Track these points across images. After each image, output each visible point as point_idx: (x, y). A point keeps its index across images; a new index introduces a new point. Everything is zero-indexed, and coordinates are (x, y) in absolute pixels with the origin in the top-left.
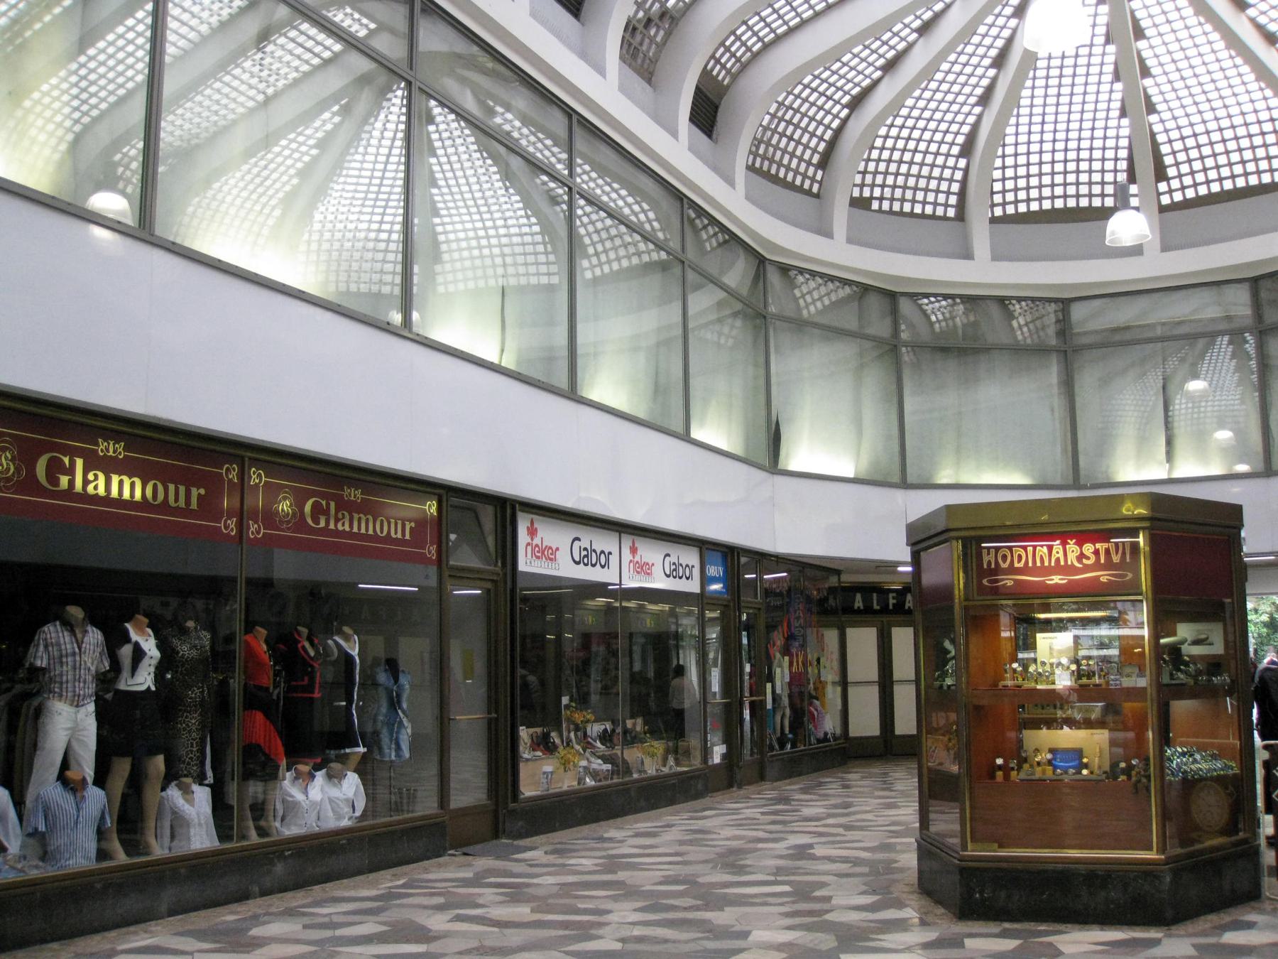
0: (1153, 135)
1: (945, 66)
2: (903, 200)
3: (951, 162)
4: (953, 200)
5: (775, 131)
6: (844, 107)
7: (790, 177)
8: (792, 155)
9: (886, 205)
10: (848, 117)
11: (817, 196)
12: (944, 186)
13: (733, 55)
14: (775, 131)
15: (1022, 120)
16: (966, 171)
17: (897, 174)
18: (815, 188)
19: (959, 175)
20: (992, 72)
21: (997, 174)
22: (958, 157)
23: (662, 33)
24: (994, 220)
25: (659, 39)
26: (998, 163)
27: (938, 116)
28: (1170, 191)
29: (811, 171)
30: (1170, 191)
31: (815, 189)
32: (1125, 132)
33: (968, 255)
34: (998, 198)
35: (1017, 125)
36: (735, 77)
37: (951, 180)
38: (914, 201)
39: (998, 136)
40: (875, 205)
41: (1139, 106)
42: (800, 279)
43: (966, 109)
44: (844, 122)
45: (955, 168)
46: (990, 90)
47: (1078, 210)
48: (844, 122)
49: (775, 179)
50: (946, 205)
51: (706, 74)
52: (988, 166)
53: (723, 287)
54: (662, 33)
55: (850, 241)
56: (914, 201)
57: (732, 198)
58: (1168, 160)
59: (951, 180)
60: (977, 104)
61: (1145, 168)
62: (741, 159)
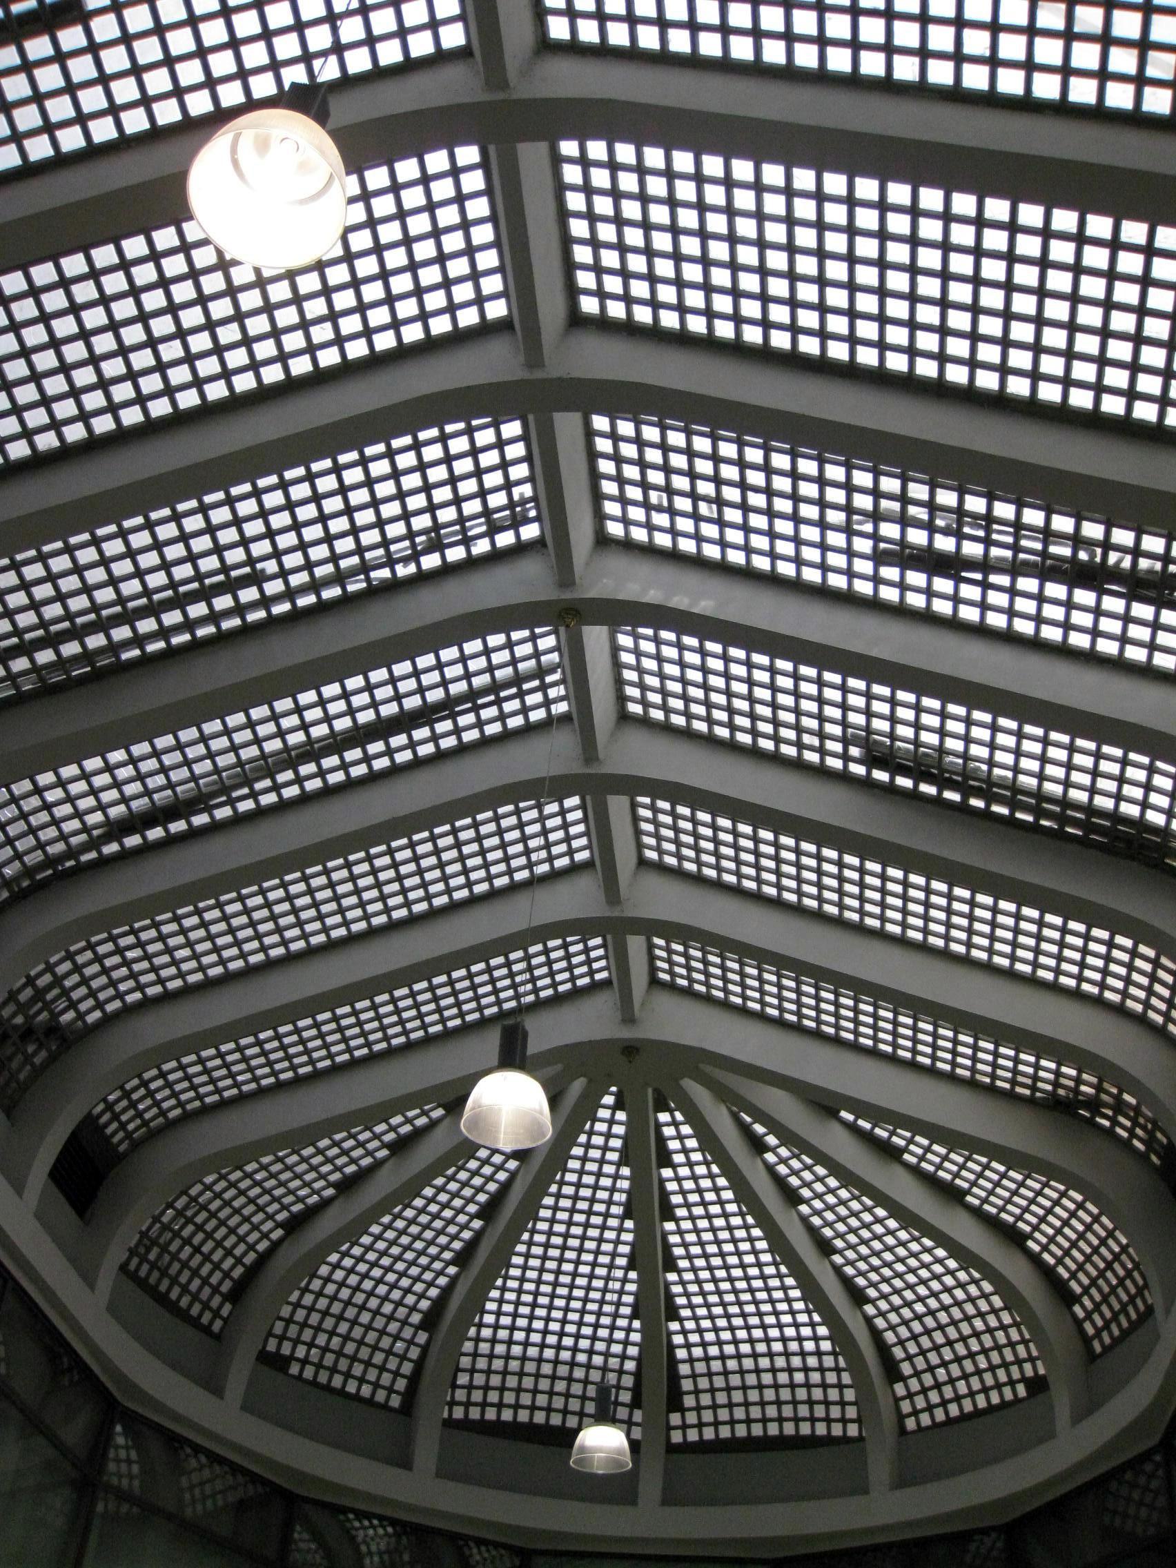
2: (333, 1370)
3: (407, 1333)
4: (401, 1384)
5: (177, 1234)
6: (278, 1225)
7: (184, 1302)
8: (195, 1273)
9: (309, 1373)
10: (281, 1241)
13: (139, 1115)
14: (177, 1234)
16: (425, 1349)
17: (332, 1333)
18: (217, 1326)
19: (414, 1353)
22: (418, 1328)
23: (43, 1054)
24: (449, 1423)
25: (37, 1060)
28: (684, 1427)
29: (217, 1300)
33: (405, 1463)
36: (136, 1145)
37: (403, 1358)
38: (348, 1375)
40: (294, 1369)
41: (655, 1308)
42: (193, 1463)
45: (411, 1342)
49: (162, 1299)
50: (390, 1390)
51: (89, 1124)
53: (56, 1443)
54: (43, 1054)
56: (348, 1375)
57: (87, 1308)
58: (687, 1385)
59: (403, 1358)
61: (657, 1392)
62: (116, 1254)
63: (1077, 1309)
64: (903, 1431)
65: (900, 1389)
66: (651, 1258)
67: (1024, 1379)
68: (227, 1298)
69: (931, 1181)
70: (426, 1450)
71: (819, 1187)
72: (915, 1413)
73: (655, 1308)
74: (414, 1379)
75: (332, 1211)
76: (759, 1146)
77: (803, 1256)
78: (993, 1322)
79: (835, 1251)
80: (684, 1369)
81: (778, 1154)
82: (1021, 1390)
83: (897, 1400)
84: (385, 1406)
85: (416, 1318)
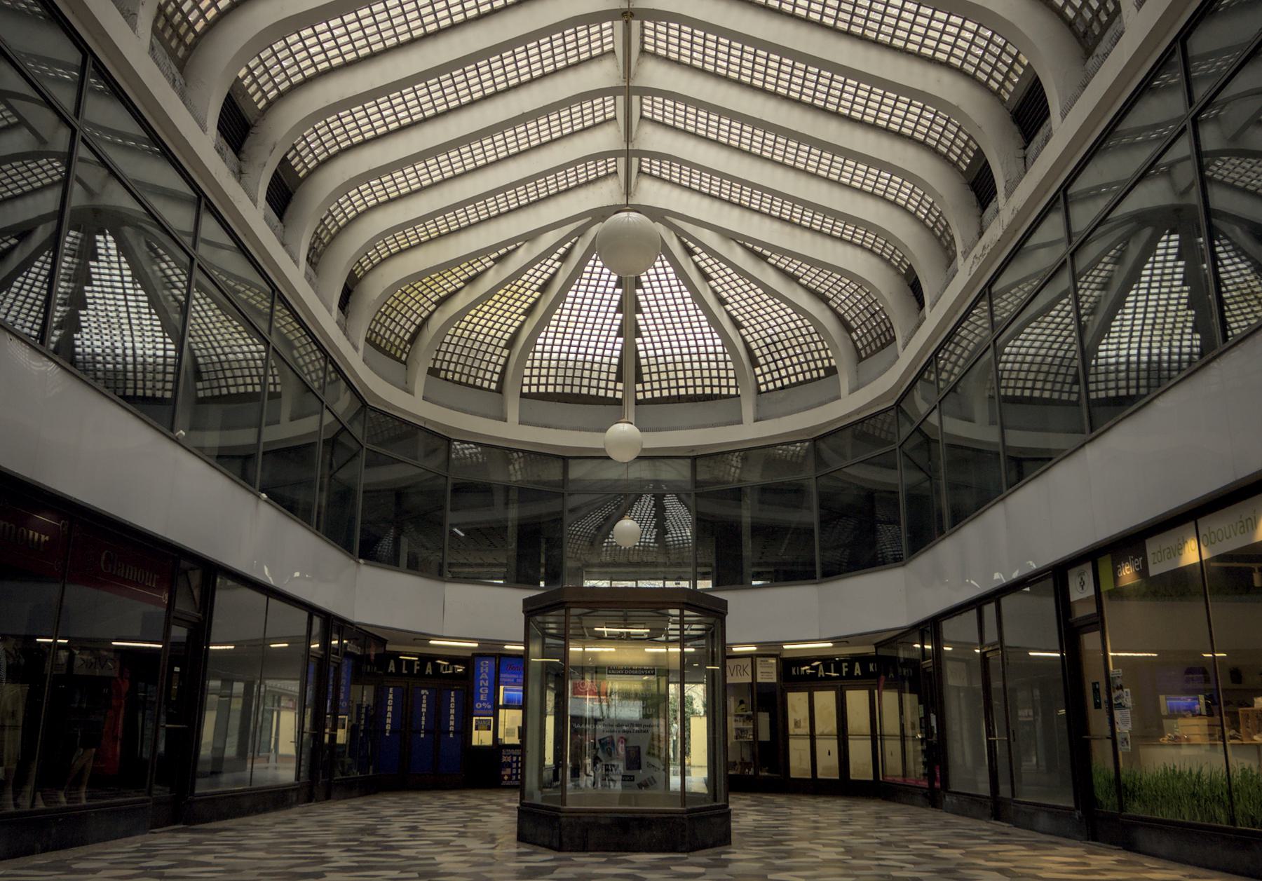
0: (637, 351)
1: (496, 297)
4: (496, 377)
11: (405, 363)
12: (491, 367)
15: (581, 288)
16: (507, 359)
20: (537, 295)
21: (527, 372)
24: (523, 395)
26: (529, 363)
27: (495, 318)
28: (644, 391)
30: (644, 391)
31: (404, 357)
32: (618, 346)
34: (526, 381)
35: (594, 267)
37: (496, 364)
39: (532, 341)
40: (443, 374)
41: (630, 330)
43: (514, 316)
44: (432, 313)
46: (533, 306)
47: (580, 395)
48: (432, 313)
52: (521, 365)
55: (424, 398)
58: (645, 370)
60: (558, 260)
61: (630, 372)
63: (854, 335)
64: (759, 392)
65: (758, 371)
66: (629, 306)
67: (823, 367)
68: (407, 342)
69: (783, 272)
70: (513, 408)
71: (722, 273)
72: (766, 383)
73: (630, 330)
74: (502, 374)
75: (462, 294)
76: (690, 252)
77: (711, 308)
78: (809, 339)
79: (743, 327)
80: (644, 362)
81: (701, 257)
82: (822, 373)
83: (756, 376)
84: (488, 389)
85: (502, 343)
